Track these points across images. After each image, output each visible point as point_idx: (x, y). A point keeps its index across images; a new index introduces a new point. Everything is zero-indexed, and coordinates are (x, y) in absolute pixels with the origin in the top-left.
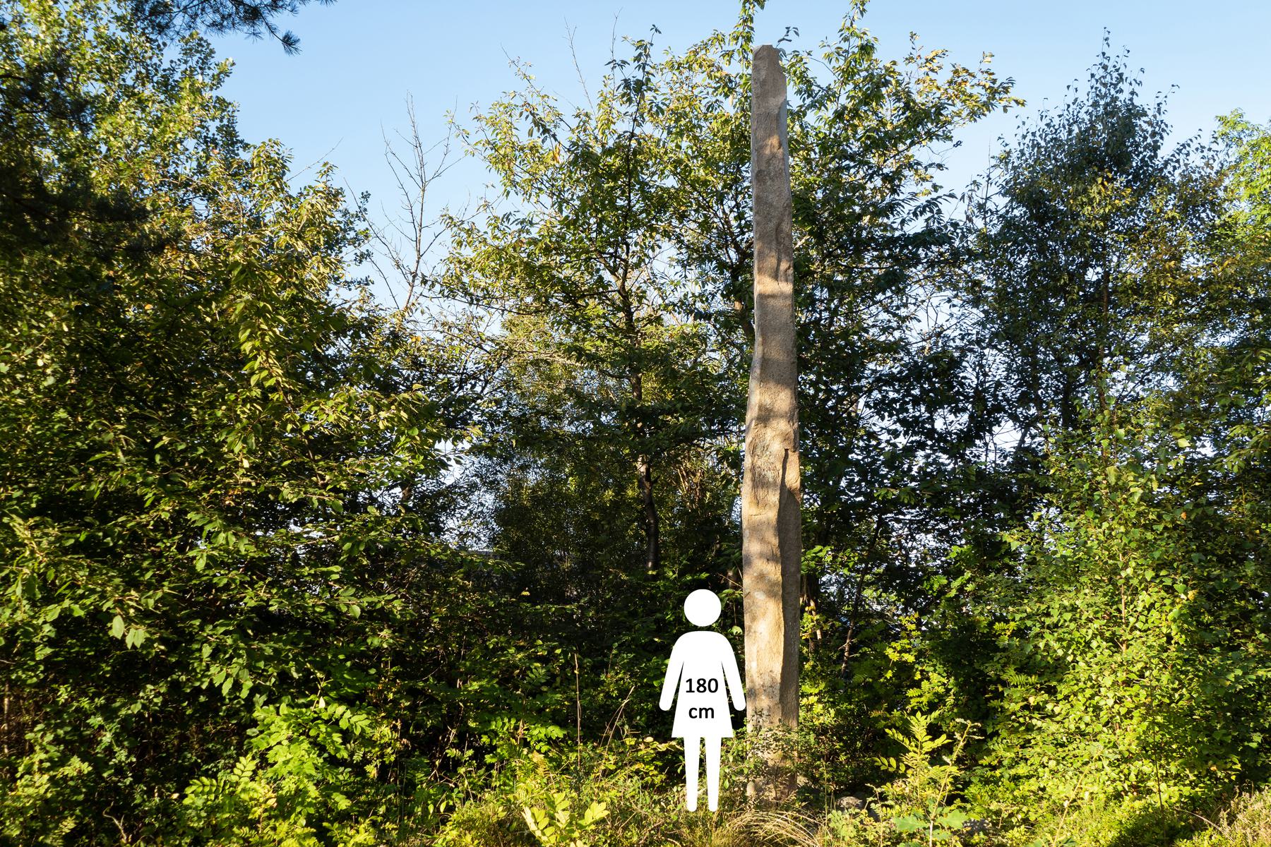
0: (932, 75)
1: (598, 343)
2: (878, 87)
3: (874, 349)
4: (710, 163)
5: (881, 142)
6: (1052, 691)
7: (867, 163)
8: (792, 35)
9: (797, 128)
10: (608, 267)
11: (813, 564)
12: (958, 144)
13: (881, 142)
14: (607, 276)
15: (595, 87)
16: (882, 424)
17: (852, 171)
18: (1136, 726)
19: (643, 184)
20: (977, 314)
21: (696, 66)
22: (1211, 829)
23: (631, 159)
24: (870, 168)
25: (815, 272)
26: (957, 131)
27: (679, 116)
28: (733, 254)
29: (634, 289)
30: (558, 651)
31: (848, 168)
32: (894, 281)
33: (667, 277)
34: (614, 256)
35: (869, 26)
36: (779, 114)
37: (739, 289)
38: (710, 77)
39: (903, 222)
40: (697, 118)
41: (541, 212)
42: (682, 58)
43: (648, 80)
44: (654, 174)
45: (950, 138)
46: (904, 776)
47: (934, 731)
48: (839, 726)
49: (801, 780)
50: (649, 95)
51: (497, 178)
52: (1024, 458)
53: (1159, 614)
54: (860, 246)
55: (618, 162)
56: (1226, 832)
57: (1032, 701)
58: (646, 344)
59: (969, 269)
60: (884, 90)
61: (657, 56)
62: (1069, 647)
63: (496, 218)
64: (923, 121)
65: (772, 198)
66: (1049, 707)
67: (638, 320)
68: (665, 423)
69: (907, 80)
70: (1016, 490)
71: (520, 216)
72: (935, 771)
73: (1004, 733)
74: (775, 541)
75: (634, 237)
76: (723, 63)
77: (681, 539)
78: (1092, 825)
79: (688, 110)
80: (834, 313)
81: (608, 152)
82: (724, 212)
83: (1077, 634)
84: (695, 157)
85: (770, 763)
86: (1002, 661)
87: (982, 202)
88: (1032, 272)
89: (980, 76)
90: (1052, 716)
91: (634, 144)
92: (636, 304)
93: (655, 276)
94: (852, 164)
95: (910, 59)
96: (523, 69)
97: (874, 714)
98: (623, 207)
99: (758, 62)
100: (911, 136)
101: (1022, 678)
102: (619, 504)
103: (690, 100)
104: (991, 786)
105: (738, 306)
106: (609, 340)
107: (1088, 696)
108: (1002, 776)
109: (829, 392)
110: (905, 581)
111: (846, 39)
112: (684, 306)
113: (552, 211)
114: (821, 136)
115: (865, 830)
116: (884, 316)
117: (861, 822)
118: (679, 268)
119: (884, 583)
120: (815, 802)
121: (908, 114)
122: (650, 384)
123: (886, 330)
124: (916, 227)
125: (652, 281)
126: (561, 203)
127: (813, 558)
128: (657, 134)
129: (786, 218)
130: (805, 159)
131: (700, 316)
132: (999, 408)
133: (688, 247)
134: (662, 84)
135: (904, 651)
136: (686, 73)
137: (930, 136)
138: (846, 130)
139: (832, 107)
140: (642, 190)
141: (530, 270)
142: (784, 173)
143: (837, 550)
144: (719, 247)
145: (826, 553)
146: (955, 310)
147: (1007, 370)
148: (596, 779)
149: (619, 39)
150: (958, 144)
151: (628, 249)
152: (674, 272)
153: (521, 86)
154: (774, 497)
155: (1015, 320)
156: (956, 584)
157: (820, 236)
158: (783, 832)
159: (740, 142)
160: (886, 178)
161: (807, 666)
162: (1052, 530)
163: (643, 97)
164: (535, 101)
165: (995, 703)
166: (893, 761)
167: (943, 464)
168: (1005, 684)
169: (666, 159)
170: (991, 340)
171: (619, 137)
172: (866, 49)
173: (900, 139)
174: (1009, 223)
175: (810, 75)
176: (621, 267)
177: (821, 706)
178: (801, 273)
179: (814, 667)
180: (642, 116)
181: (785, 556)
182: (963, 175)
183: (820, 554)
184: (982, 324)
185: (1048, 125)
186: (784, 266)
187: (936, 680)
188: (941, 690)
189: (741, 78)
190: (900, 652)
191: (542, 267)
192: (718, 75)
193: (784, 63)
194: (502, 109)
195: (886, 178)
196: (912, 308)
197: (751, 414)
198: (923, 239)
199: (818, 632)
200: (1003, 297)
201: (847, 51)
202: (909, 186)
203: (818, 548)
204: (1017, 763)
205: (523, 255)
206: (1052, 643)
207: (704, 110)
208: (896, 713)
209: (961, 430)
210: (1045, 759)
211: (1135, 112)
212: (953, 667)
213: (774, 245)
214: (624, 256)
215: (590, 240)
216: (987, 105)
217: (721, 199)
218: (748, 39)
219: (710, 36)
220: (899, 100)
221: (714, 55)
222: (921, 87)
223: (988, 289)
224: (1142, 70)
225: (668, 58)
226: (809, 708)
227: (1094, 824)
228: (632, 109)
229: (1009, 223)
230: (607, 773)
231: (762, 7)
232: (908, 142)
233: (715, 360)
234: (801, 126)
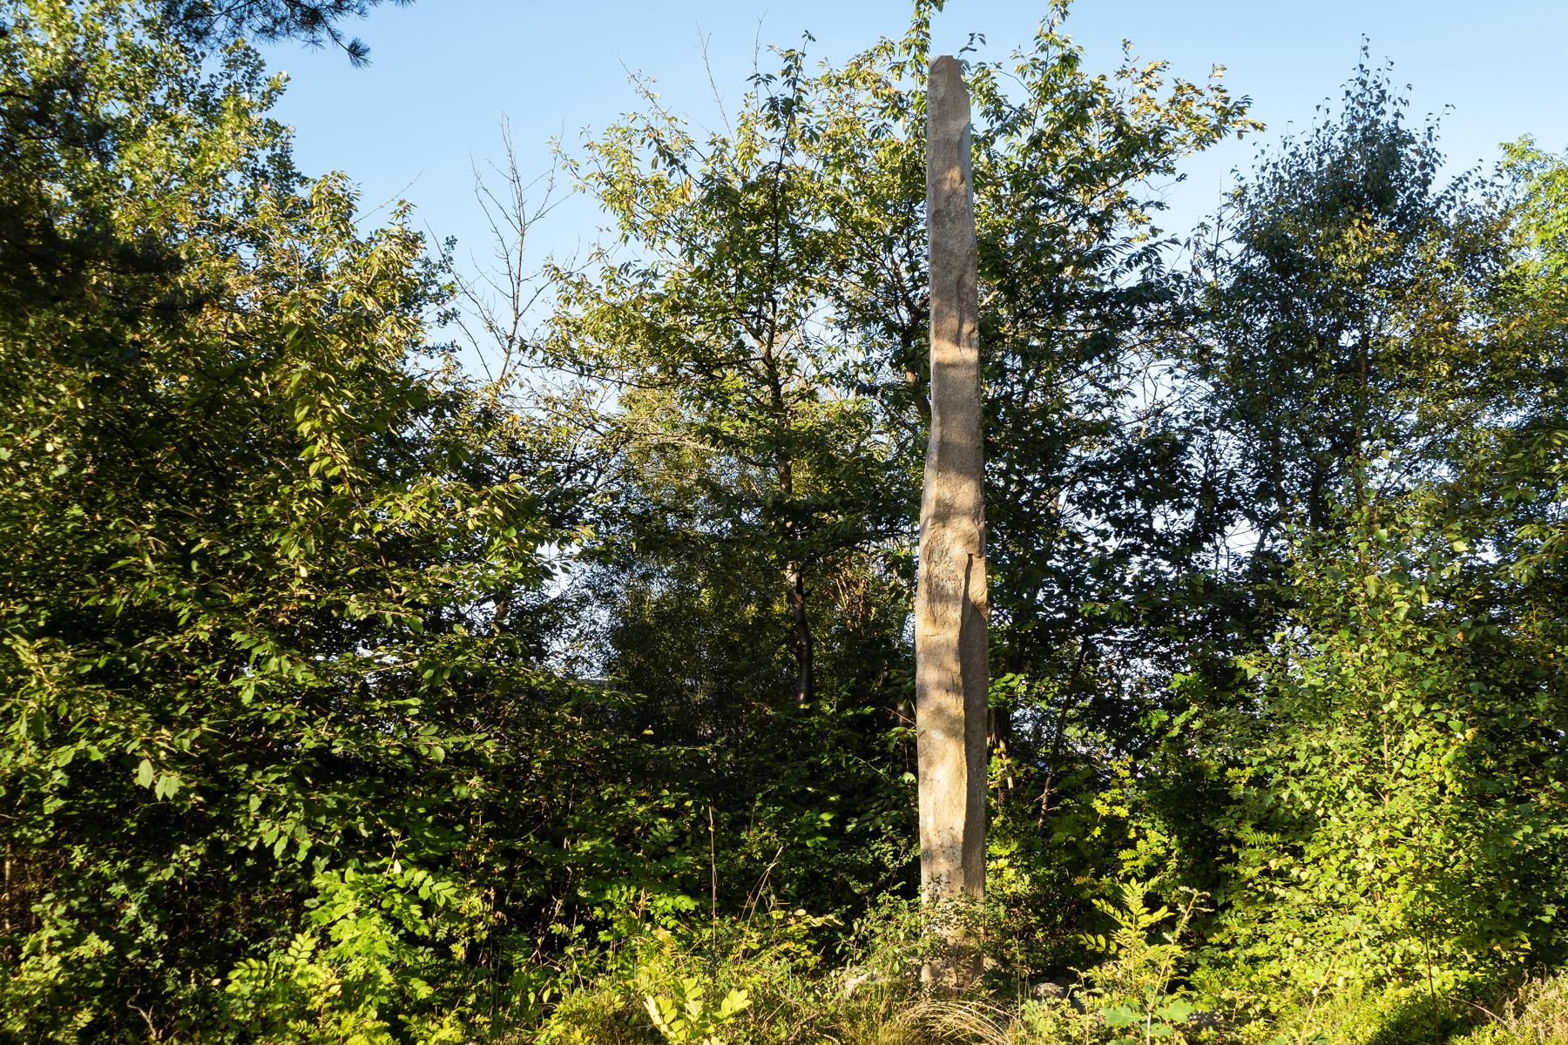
0: (1150, 93)
1: (738, 423)
2: (1083, 108)
3: (1078, 430)
4: (876, 202)
5: (1087, 175)
6: (1298, 853)
7: (1070, 201)
8: (977, 43)
9: (983, 158)
10: (749, 329)
11: (1002, 696)
12: (1182, 177)
13: (1087, 175)
14: (749, 340)
16: (1088, 524)
17: (1051, 211)
18: (1402, 896)
19: (794, 227)
20: (1205, 387)
21: (858, 82)
22: (1493, 1023)
23: (779, 196)
24: (1074, 207)
25: (1005, 336)
26: (1181, 162)
27: (838, 143)
29: (782, 357)
30: (689, 803)
31: (1046, 207)
32: (1103, 347)
33: (822, 343)
34: (758, 315)
35: (1072, 32)
36: (960, 141)
37: (912, 356)
38: (876, 94)
39: (1114, 274)
41: (667, 262)
42: (842, 71)
43: (800, 98)
44: (806, 214)
45: (1172, 171)
46: (1116, 957)
47: (1152, 902)
48: (1035, 896)
49: (989, 963)
50: (800, 117)
51: (613, 220)
52: (1264, 565)
53: (1430, 758)
54: (1060, 304)
55: (762, 200)
56: (1513, 1027)
57: (1274, 864)
58: (797, 424)
59: (1196, 332)
60: (1090, 111)
61: (811, 70)
62: (1318, 798)
63: (612, 269)
64: (1138, 149)
65: (953, 244)
66: (1295, 872)
67: (787, 395)
68: (821, 522)
69: (1119, 99)
70: (1253, 605)
71: (642, 267)
72: (1153, 951)
73: (1238, 905)
74: (956, 668)
75: (783, 292)
76: (892, 78)
77: (840, 666)
78: (1348, 1018)
79: (848, 135)
80: (1029, 386)
81: (750, 188)
82: (893, 262)
83: (1328, 783)
84: (858, 194)
85: (950, 942)
86: (1236, 816)
87: (1211, 249)
88: (1273, 336)
89: (1208, 93)
90: (1298, 883)
91: (782, 177)
92: (784, 375)
94: (1051, 202)
95: (1122, 73)
96: (645, 85)
97: (1079, 881)
100: (1125, 168)
101: (1261, 837)
104: (1223, 970)
105: (910, 377)
106: (752, 420)
107: (1342, 858)
108: (1236, 958)
109: (1022, 483)
110: (1116, 717)
111: (1044, 49)
113: (681, 261)
114: (1013, 167)
115: (1067, 1024)
116: (1091, 390)
117: (1063, 1014)
118: (837, 331)
119: (1090, 719)
120: (1006, 989)
121: (1120, 140)
122: (802, 474)
123: (1093, 407)
124: (1130, 280)
125: (804, 347)
126: (692, 250)
127: (1003, 689)
128: (811, 165)
129: (969, 269)
130: (994, 196)
131: (863, 389)
132: (1232, 504)
133: (848, 305)
134: (816, 104)
135: (1115, 803)
136: (847, 90)
137: (1148, 168)
138: (1044, 160)
139: (1026, 133)
140: (792, 234)
141: (654, 333)
142: (967, 213)
143: (1032, 679)
144: (887, 305)
145: (1019, 683)
146: (1178, 382)
147: (1242, 456)
148: (736, 961)
149: (764, 48)
150: (1182, 177)
151: (775, 307)
152: (832, 336)
153: (643, 106)
154: (955, 614)
155: (1252, 395)
156: (1179, 720)
157: (1011, 291)
158: (966, 1026)
159: (912, 176)
160: (1093, 220)
161: (996, 822)
162: (1298, 654)
163: (793, 119)
164: (660, 125)
165: (1227, 867)
166: (1101, 939)
167: (1163, 572)
170: (1223, 419)
171: (764, 169)
172: (1069, 61)
173: (1111, 172)
174: (1245, 276)
175: (999, 92)
176: (766, 330)
177: (1012, 871)
178: (989, 337)
179: (1004, 823)
180: (792, 143)
181: (968, 686)
182: (1188, 216)
183: (1012, 684)
184: (1212, 400)
185: (1292, 154)
186: (967, 328)
187: (1155, 839)
188: (1161, 851)
189: (914, 96)
190: (1110, 805)
191: (668, 329)
192: (886, 92)
193: (968, 77)
194: (619, 134)
195: (1093, 220)
196: (1125, 380)
197: (927, 511)
198: (1143, 294)
199: (1010, 780)
200: (1237, 366)
201: (1045, 63)
202: (1121, 229)
203: (1009, 676)
204: (1255, 941)
205: (645, 315)
206: (1298, 793)
207: (869, 136)
208: (1105, 880)
209: (1186, 531)
210: (1289, 937)
211: (1400, 138)
212: (1176, 823)
213: (955, 302)
214: (770, 316)
215: (728, 295)
216: (1218, 130)
217: (889, 245)
218: (923, 48)
219: (872, 44)
220: (1109, 124)
221: (881, 68)
222: (1136, 107)
223: (1218, 356)
224: (1409, 87)
225: (824, 72)
226: (999, 873)
227: (1350, 1017)
228: (780, 134)
229: (1245, 276)
230: (749, 954)
231: (940, 9)
232: (1120, 175)
233: (882, 444)
234: (988, 155)
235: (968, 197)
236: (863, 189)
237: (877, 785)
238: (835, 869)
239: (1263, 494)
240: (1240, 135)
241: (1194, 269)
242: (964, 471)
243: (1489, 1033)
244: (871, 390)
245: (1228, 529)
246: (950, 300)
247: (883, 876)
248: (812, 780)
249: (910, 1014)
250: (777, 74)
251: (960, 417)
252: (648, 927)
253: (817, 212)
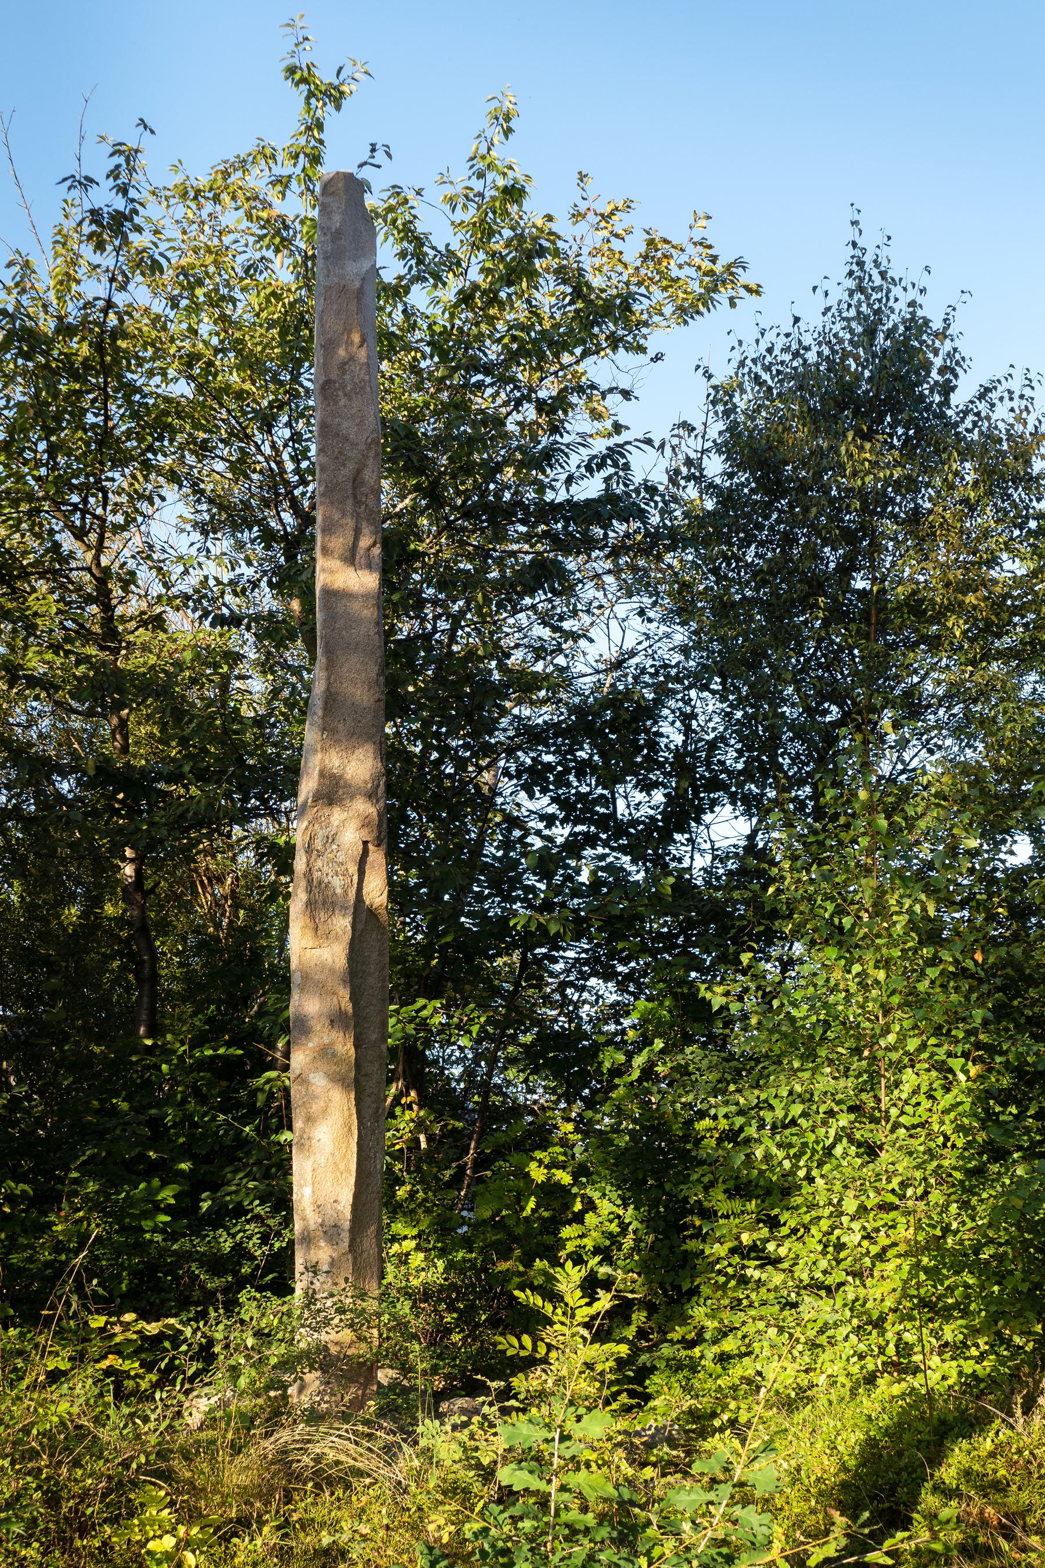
1: (49, 656)
3: (525, 684)
4: (251, 364)
5: (538, 347)
6: (774, 1223)
7: (513, 380)
8: (380, 157)
10: (70, 527)
11: (410, 1029)
12: (657, 358)
13: (538, 347)
14: (67, 542)
17: (489, 391)
18: (895, 1270)
19: (131, 389)
20: (680, 636)
21: (225, 198)
22: (998, 1421)
25: (425, 554)
31: (480, 386)
35: (516, 156)
37: (293, 577)
38: (249, 217)
39: (569, 481)
40: (227, 285)
42: (203, 181)
43: (135, 212)
46: (545, 1361)
47: (591, 1286)
53: (932, 1099)
54: (497, 515)
55: (85, 350)
56: (1019, 1428)
57: (746, 1238)
58: (133, 662)
61: (155, 170)
62: (798, 1157)
64: (604, 317)
65: (347, 426)
67: (123, 619)
70: (735, 917)
72: (594, 1351)
73: (706, 1290)
74: (344, 995)
76: (272, 195)
77: (194, 989)
78: (827, 1425)
79: (212, 269)
80: (456, 620)
82: (273, 446)
83: (811, 1138)
85: (334, 1350)
86: (706, 1179)
89: (690, 249)
90: (775, 1262)
91: (112, 320)
92: (117, 592)
93: (151, 547)
94: (488, 380)
95: (577, 216)
97: (503, 1266)
98: (94, 426)
99: (328, 200)
100: (583, 342)
101: (736, 1205)
102: (92, 924)
103: (218, 253)
104: (686, 1372)
107: (825, 1228)
108: (702, 1357)
109: (445, 750)
110: (568, 1059)
111: (481, 175)
112: (199, 600)
114: (438, 329)
115: (477, 1449)
117: (472, 1437)
118: (196, 536)
119: (533, 1060)
121: (580, 305)
123: (540, 652)
124: (591, 488)
127: (412, 1020)
128: (159, 306)
129: (370, 462)
133: (211, 501)
136: (208, 207)
137: (614, 342)
138: (477, 324)
142: (368, 387)
144: (266, 503)
150: (657, 358)
151: (106, 498)
152: (187, 543)
154: (343, 924)
155: (740, 646)
156: (639, 1061)
157: (434, 495)
158: (342, 1458)
159: (294, 328)
161: (402, 1192)
162: (812, 974)
165: (692, 1245)
168: (709, 1214)
172: (514, 193)
173: (561, 346)
175: (420, 227)
176: (97, 533)
177: (421, 1256)
178: (396, 556)
179: (412, 1194)
181: (359, 1021)
182: (659, 408)
186: (365, 542)
187: (606, 1208)
188: (614, 1227)
189: (302, 222)
192: (264, 215)
195: (541, 406)
197: (308, 786)
198: (612, 506)
199: (422, 1138)
201: (481, 195)
202: (578, 423)
206: (774, 1150)
211: (916, 325)
212: (633, 1190)
214: (99, 511)
215: (38, 479)
216: (706, 300)
217: (267, 424)
218: (315, 160)
219: (246, 147)
221: (257, 179)
222: (597, 261)
224: (927, 269)
225: (179, 179)
226: (403, 1259)
227: (832, 1424)
230: (55, 1376)
231: (338, 108)
232: (578, 351)
235: (371, 368)
240: (733, 304)
241: (670, 480)
242: (355, 736)
243: (991, 1434)
248: (154, 1142)
249: (268, 1445)
251: (354, 659)
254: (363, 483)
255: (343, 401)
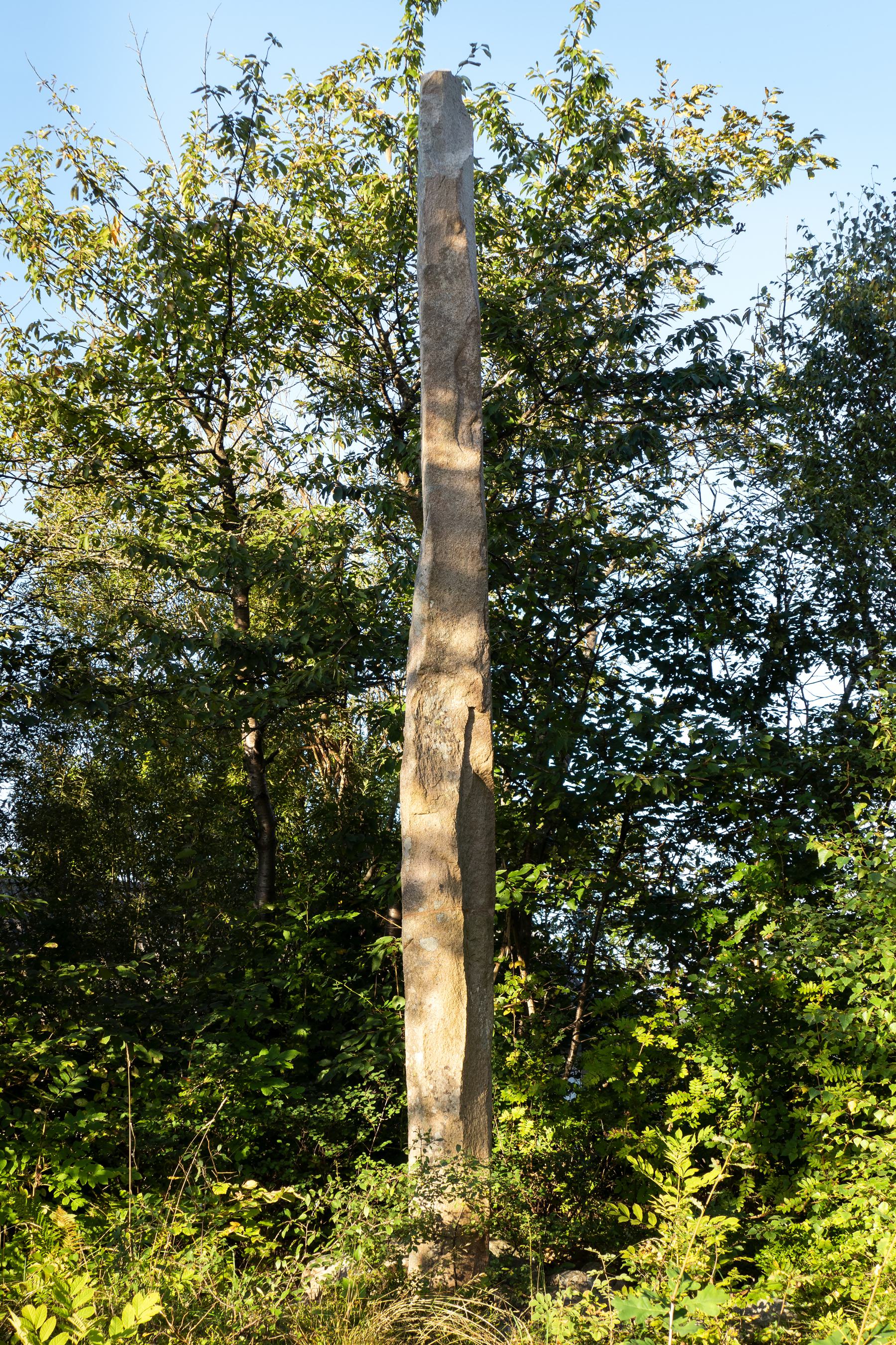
0: (697, 124)
2: (615, 142)
3: (620, 550)
4: (362, 255)
5: (625, 226)
7: (602, 258)
8: (480, 56)
9: (494, 202)
10: (194, 410)
12: (739, 230)
13: (625, 226)
14: (193, 426)
15: (178, 128)
16: (634, 668)
17: (580, 270)
19: (253, 282)
20: (771, 497)
21: (334, 101)
23: (230, 246)
24: (607, 265)
25: (522, 427)
26: (738, 210)
27: (310, 176)
28: (394, 395)
29: (237, 449)
30: (105, 1040)
31: (572, 266)
32: (647, 443)
33: (289, 428)
34: (207, 396)
36: (459, 180)
37: (400, 453)
38: (356, 116)
39: (660, 351)
40: (337, 180)
41: (91, 325)
43: (261, 118)
44: (269, 267)
45: (727, 220)
47: (702, 1158)
48: (563, 1155)
49: (496, 1247)
50: (262, 143)
51: (19, 267)
52: (849, 723)
58: (260, 539)
59: (763, 427)
60: (623, 147)
61: (275, 83)
63: (17, 332)
64: (687, 195)
65: (450, 309)
66: (879, 1115)
68: (283, 665)
69: (658, 131)
71: (54, 329)
73: (814, 1162)
75: (240, 366)
81: (197, 230)
84: (335, 242)
85: (447, 1219)
87: (777, 323)
88: (851, 436)
91: (237, 218)
94: (579, 259)
96: (62, 95)
97: (614, 1134)
99: (428, 97)
100: (669, 218)
102: (218, 794)
104: (796, 1247)
105: (403, 479)
106: (195, 532)
109: (547, 616)
110: (668, 918)
111: (568, 67)
112: (318, 480)
113: (105, 322)
115: (588, 1324)
116: (638, 498)
117: (583, 1311)
120: (513, 1284)
122: (262, 603)
124: (681, 359)
125: (265, 435)
126: (123, 311)
128: (275, 205)
129: (471, 342)
131: (342, 493)
132: (805, 643)
134: (282, 126)
135: (661, 1030)
136: (321, 112)
138: (568, 207)
139: (546, 172)
140: (250, 291)
141: (71, 415)
143: (559, 870)
145: (539, 875)
146: (742, 491)
147: (815, 584)
148: (159, 1254)
149: (214, 55)
151: (228, 384)
153: (61, 120)
157: (530, 370)
158: (456, 1332)
159: (400, 220)
160: (630, 281)
161: (512, 1058)
163: (253, 145)
164: (83, 145)
166: (638, 1210)
167: (721, 732)
169: (287, 243)
170: (792, 537)
171: (213, 207)
172: (598, 81)
173: (653, 224)
174: (818, 356)
175: (512, 119)
177: (530, 1123)
179: (521, 1060)
180: (250, 175)
184: (778, 512)
185: (877, 206)
187: (712, 1077)
188: (720, 1094)
189: (405, 120)
190: (655, 1033)
191: (90, 410)
192: (370, 115)
193: (470, 98)
194: (25, 158)
195: (630, 281)
196: (679, 486)
198: (698, 376)
199: (530, 1003)
200: (811, 469)
202: (665, 295)
203: (527, 867)
204: (835, 1208)
205: (59, 392)
206: (881, 1013)
207: (349, 170)
208: (648, 1132)
209: (749, 679)
210: (873, 1200)
213: (452, 380)
214: (223, 398)
215: (168, 370)
218: (415, 61)
219: (352, 53)
220: (648, 162)
221: (362, 83)
222: (680, 141)
223: (791, 458)
225: (291, 86)
228: (236, 164)
229: (818, 356)
230: (182, 1242)
232: (664, 227)
233: (368, 563)
234: (500, 198)
236: (346, 238)
237: (355, 1014)
238: (302, 1123)
239: (846, 631)
244: (353, 493)
245: (802, 677)
246: (447, 377)
247: (361, 1136)
250: (231, 87)
252: (45, 1209)
253: (282, 264)
254: (464, 361)
255: (444, 285)
